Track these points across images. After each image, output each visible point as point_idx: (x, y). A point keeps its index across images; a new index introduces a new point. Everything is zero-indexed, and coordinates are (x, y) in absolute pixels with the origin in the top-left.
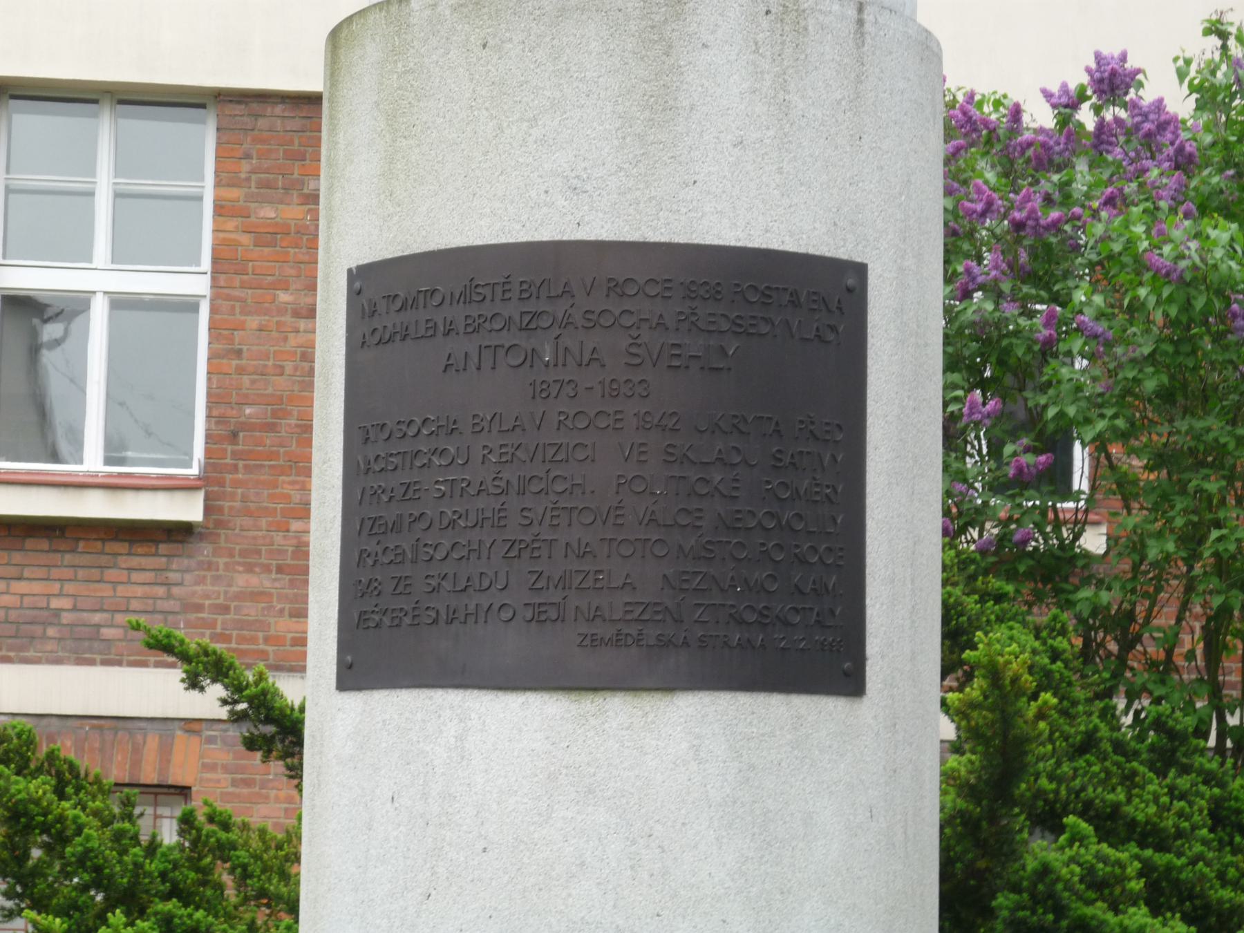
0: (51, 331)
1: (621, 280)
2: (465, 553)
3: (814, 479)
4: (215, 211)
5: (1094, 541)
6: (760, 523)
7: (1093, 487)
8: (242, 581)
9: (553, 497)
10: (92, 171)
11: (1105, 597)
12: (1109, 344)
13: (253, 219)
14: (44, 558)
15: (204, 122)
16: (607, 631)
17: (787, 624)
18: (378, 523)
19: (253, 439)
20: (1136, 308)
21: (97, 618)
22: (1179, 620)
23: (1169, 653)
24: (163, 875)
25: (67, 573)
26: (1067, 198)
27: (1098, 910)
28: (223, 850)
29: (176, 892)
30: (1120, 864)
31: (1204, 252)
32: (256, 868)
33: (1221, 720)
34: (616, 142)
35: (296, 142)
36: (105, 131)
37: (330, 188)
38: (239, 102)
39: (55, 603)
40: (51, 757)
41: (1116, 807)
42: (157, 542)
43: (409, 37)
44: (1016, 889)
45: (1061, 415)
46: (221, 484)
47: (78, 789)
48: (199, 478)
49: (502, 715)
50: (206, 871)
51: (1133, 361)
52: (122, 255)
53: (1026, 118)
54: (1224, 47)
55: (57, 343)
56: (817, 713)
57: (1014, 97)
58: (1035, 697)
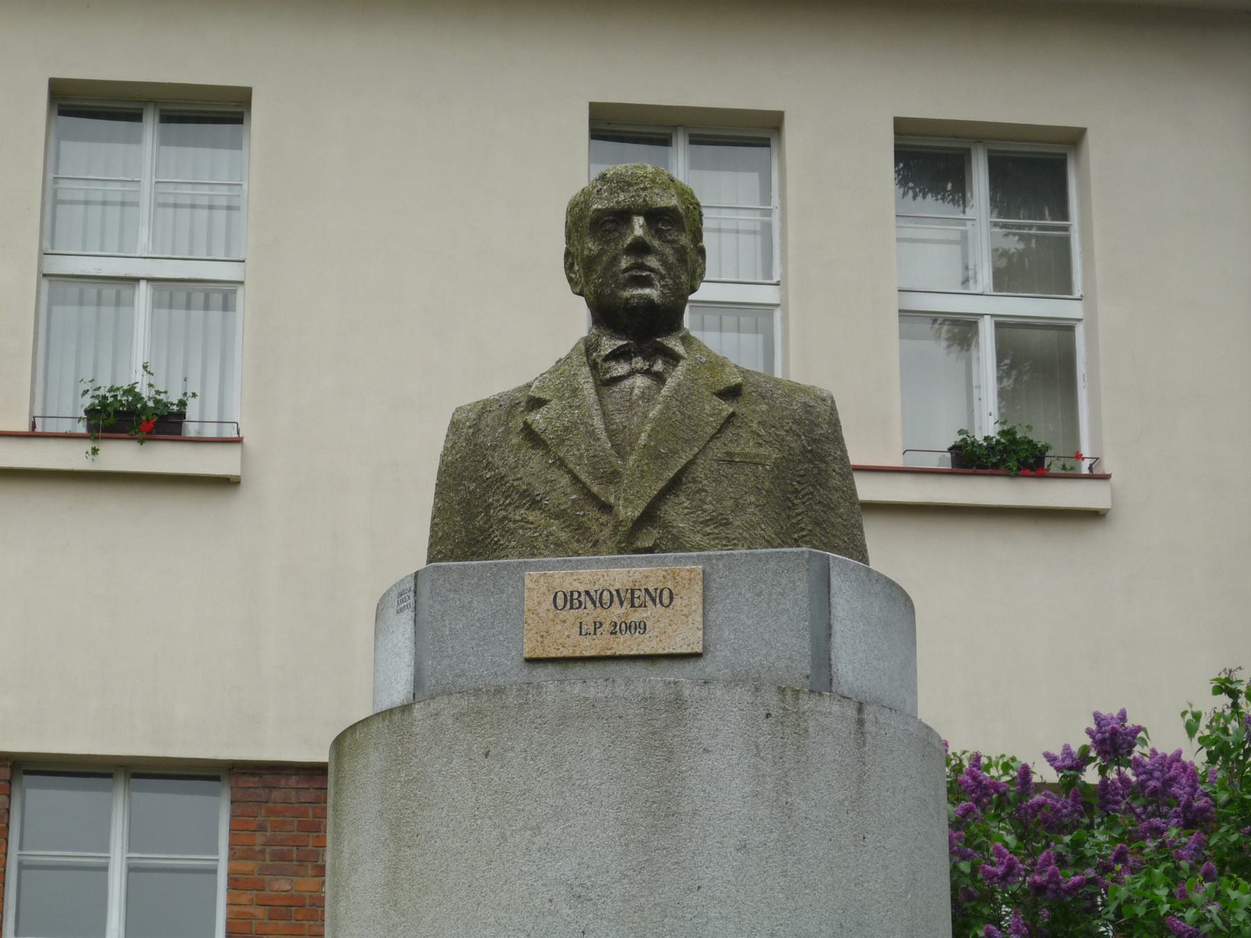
4: (229, 884)
10: (105, 847)
13: (267, 892)
15: (217, 794)
31: (1226, 911)
35: (311, 813)
37: (335, 897)
38: (252, 775)
43: (412, 747)
54: (1235, 705)
57: (1023, 759)
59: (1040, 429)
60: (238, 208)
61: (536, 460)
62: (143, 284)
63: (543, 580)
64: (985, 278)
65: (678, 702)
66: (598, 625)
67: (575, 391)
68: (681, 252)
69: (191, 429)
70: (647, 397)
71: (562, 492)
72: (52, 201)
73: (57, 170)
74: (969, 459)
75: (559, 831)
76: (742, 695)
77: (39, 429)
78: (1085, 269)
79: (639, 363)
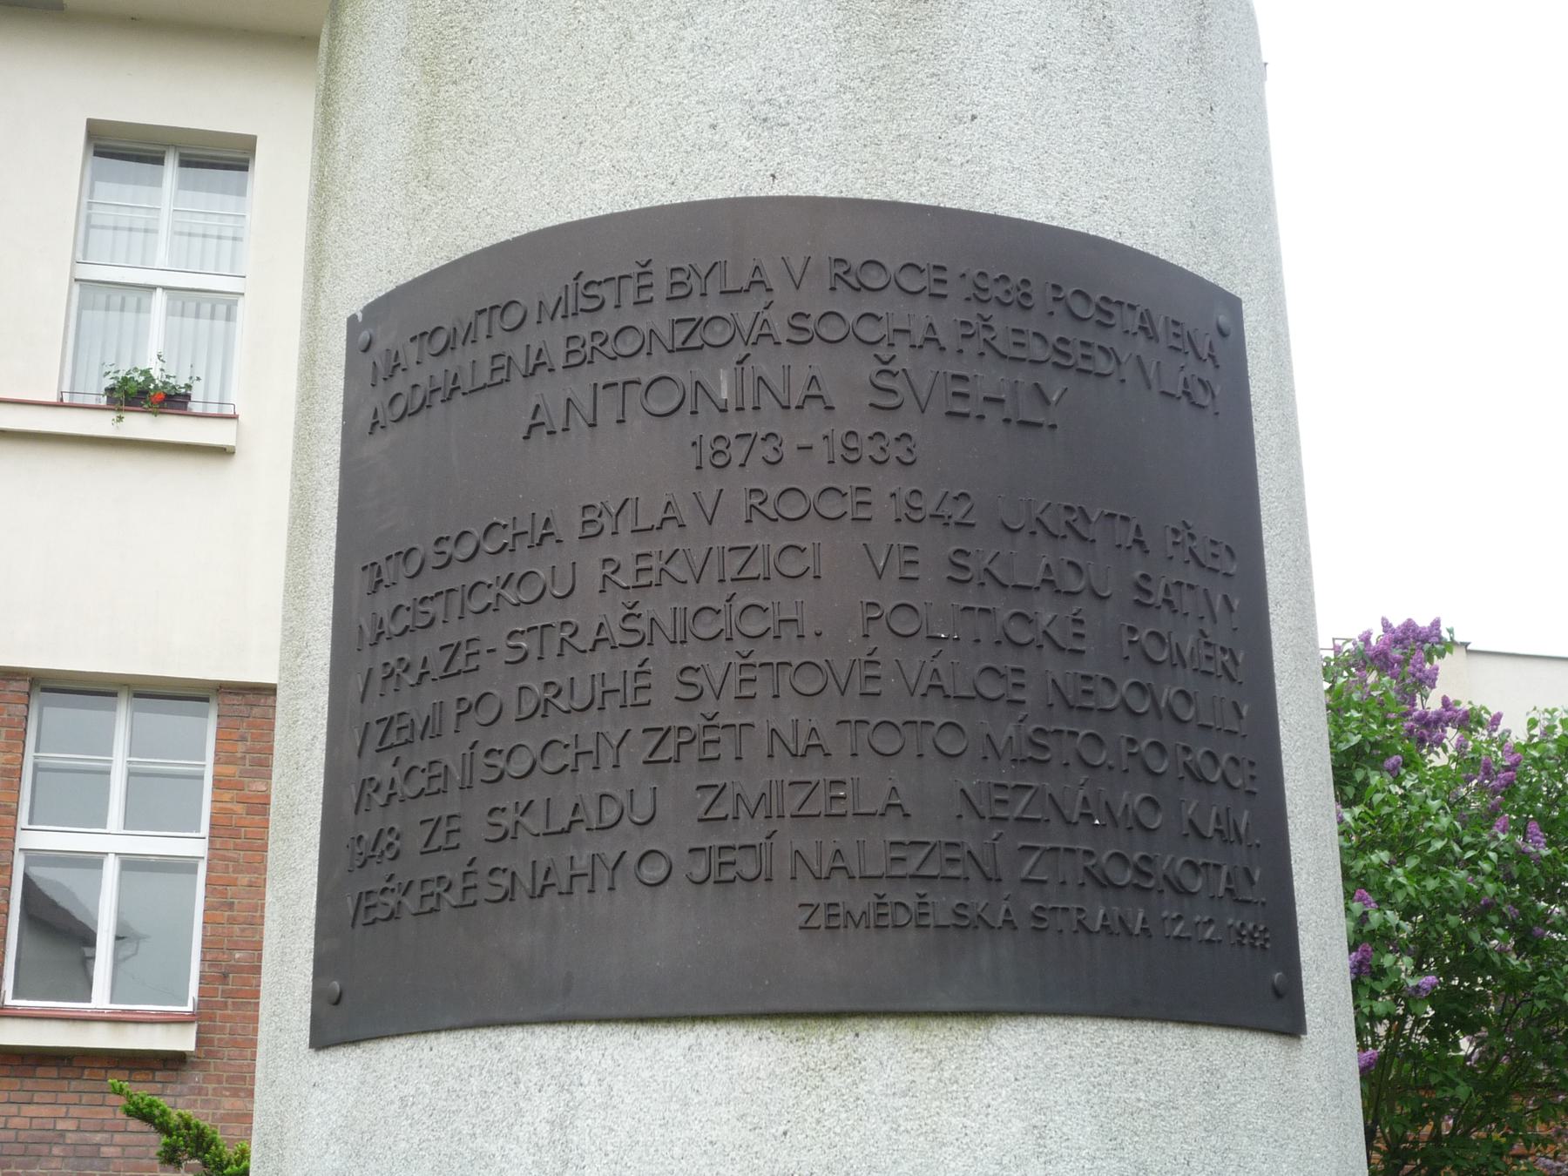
1: (856, 263)
2: (569, 758)
3: (1202, 633)
6: (1123, 702)
9: (742, 645)
14: (52, 1085)
16: (859, 900)
17: (1181, 891)
18: (396, 726)
21: (98, 1138)
25: (74, 1098)
34: (834, 47)
36: (122, 718)
39: (61, 1125)
42: (153, 1070)
46: (212, 1019)
48: (193, 1014)
49: (646, 1074)
56: (1259, 1049)
60: (241, 240)
62: (159, 291)
69: (195, 407)
72: (87, 226)
73: (91, 196)
75: (727, 18)
77: (66, 400)
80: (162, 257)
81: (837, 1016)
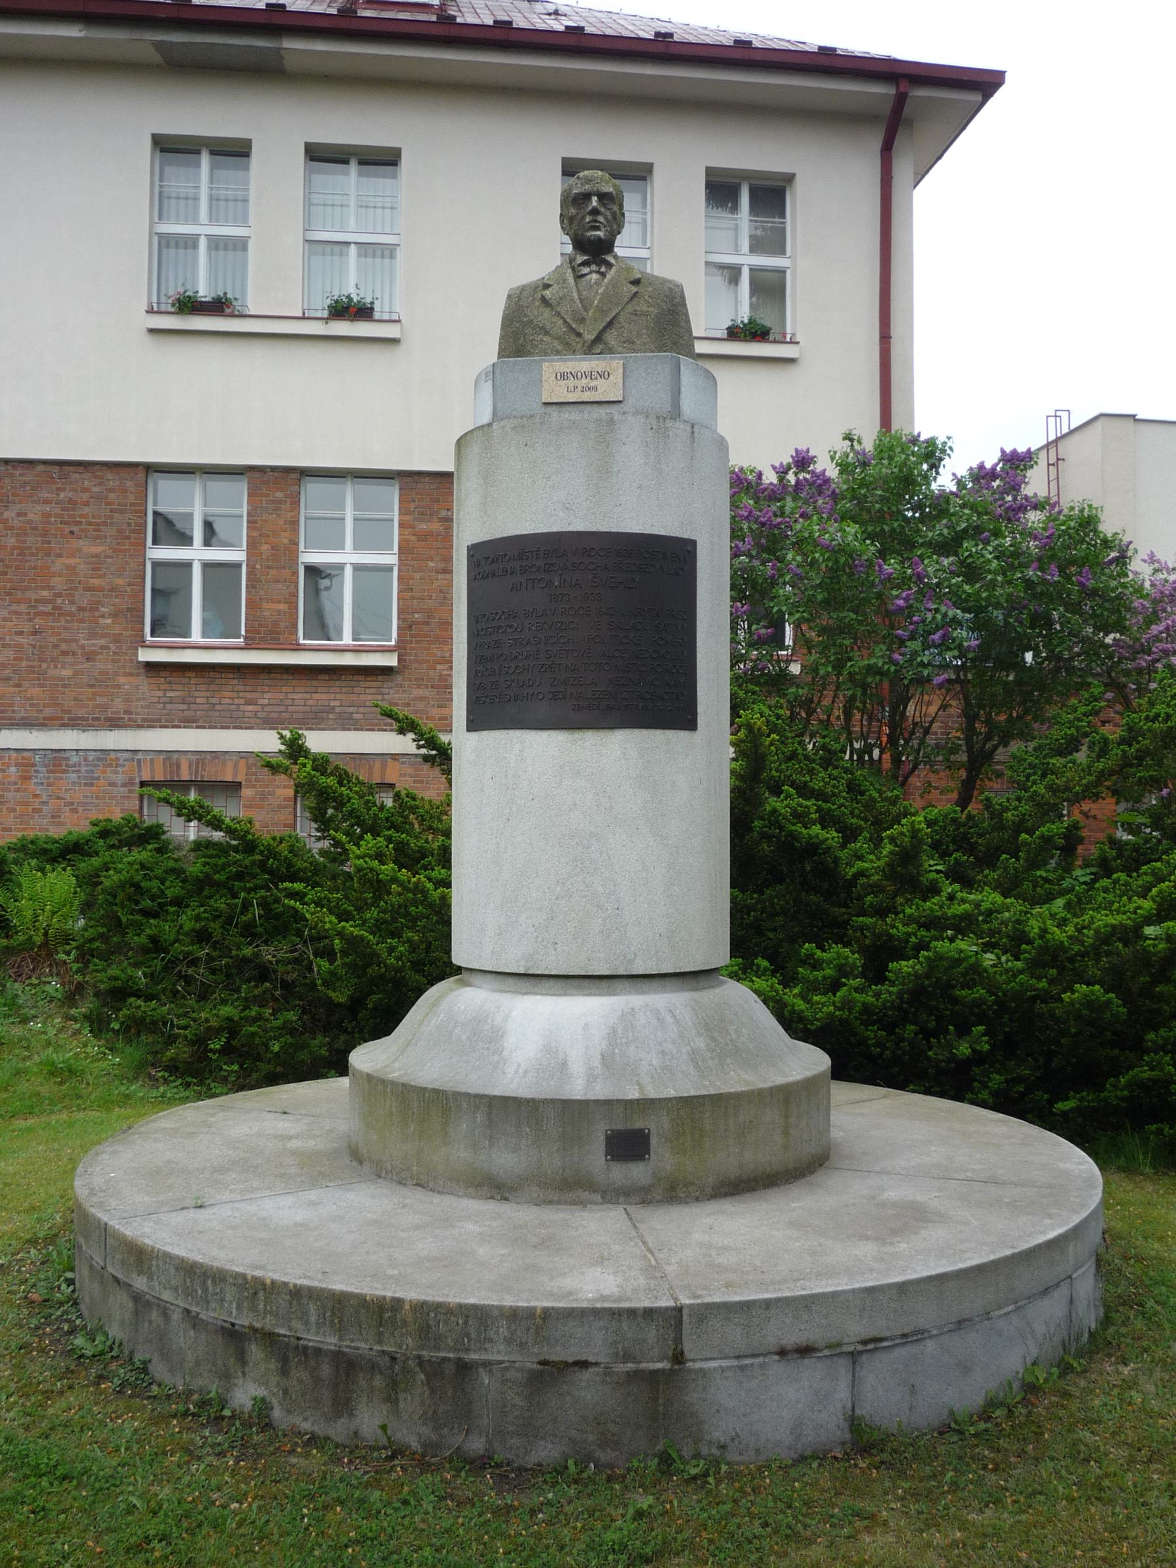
0: (324, 583)
5: (795, 669)
7: (795, 644)
8: (417, 692)
11: (801, 691)
12: (802, 579)
19: (421, 629)
20: (813, 564)
21: (351, 710)
22: (833, 702)
23: (829, 717)
24: (387, 819)
26: (783, 514)
27: (798, 828)
28: (413, 809)
29: (393, 826)
30: (807, 807)
32: (427, 817)
33: (852, 745)
36: (349, 491)
37: (458, 510)
39: (332, 704)
40: (337, 767)
41: (806, 783)
44: (762, 819)
45: (780, 610)
47: (349, 782)
50: (406, 817)
51: (813, 587)
52: (358, 546)
53: (764, 478)
54: (852, 446)
55: (327, 589)
56: (683, 735)
57: (759, 468)
58: (769, 736)
59: (767, 319)
61: (547, 313)
63: (551, 367)
64: (745, 245)
65: (612, 422)
66: (575, 388)
67: (565, 281)
68: (614, 214)
69: (377, 316)
70: (597, 283)
71: (559, 328)
72: (308, 204)
74: (734, 333)
76: (641, 419)
78: (792, 246)
79: (594, 267)
80: (352, 224)
81: (580, 729)
